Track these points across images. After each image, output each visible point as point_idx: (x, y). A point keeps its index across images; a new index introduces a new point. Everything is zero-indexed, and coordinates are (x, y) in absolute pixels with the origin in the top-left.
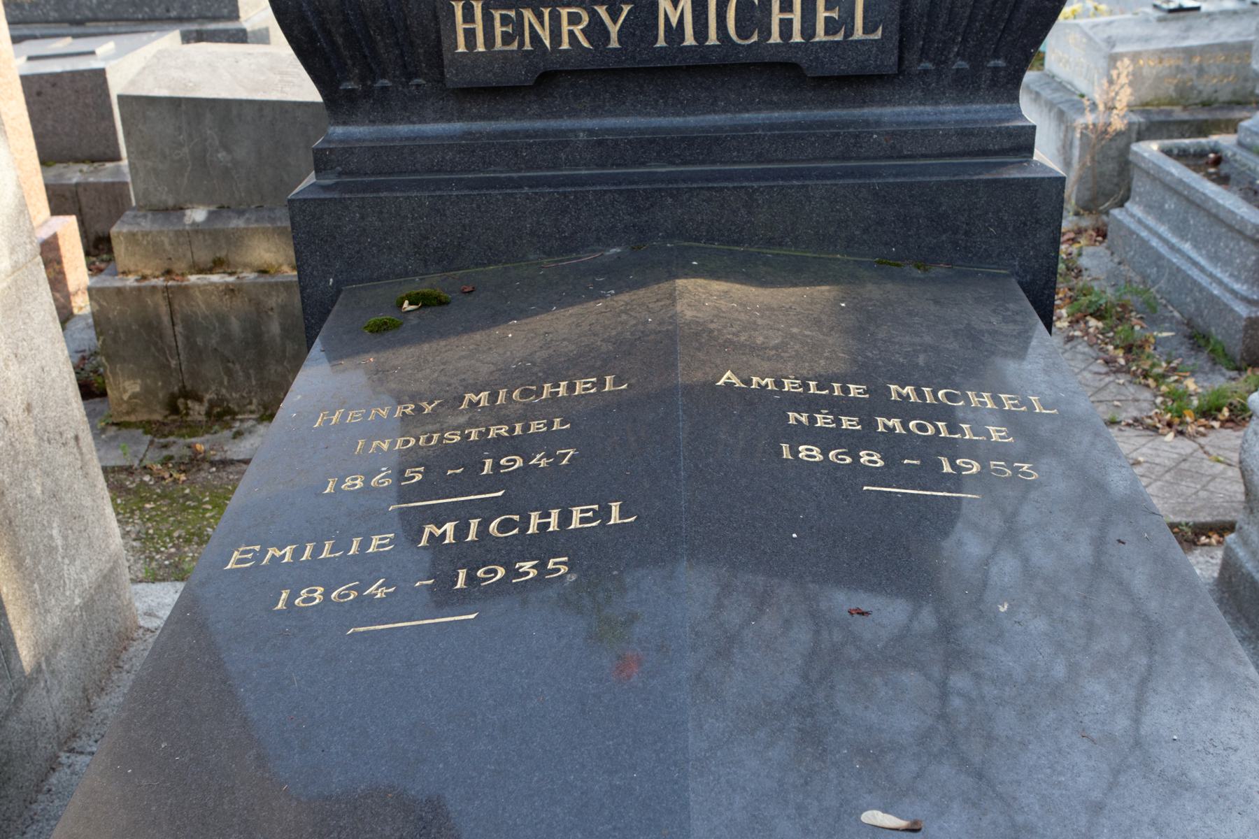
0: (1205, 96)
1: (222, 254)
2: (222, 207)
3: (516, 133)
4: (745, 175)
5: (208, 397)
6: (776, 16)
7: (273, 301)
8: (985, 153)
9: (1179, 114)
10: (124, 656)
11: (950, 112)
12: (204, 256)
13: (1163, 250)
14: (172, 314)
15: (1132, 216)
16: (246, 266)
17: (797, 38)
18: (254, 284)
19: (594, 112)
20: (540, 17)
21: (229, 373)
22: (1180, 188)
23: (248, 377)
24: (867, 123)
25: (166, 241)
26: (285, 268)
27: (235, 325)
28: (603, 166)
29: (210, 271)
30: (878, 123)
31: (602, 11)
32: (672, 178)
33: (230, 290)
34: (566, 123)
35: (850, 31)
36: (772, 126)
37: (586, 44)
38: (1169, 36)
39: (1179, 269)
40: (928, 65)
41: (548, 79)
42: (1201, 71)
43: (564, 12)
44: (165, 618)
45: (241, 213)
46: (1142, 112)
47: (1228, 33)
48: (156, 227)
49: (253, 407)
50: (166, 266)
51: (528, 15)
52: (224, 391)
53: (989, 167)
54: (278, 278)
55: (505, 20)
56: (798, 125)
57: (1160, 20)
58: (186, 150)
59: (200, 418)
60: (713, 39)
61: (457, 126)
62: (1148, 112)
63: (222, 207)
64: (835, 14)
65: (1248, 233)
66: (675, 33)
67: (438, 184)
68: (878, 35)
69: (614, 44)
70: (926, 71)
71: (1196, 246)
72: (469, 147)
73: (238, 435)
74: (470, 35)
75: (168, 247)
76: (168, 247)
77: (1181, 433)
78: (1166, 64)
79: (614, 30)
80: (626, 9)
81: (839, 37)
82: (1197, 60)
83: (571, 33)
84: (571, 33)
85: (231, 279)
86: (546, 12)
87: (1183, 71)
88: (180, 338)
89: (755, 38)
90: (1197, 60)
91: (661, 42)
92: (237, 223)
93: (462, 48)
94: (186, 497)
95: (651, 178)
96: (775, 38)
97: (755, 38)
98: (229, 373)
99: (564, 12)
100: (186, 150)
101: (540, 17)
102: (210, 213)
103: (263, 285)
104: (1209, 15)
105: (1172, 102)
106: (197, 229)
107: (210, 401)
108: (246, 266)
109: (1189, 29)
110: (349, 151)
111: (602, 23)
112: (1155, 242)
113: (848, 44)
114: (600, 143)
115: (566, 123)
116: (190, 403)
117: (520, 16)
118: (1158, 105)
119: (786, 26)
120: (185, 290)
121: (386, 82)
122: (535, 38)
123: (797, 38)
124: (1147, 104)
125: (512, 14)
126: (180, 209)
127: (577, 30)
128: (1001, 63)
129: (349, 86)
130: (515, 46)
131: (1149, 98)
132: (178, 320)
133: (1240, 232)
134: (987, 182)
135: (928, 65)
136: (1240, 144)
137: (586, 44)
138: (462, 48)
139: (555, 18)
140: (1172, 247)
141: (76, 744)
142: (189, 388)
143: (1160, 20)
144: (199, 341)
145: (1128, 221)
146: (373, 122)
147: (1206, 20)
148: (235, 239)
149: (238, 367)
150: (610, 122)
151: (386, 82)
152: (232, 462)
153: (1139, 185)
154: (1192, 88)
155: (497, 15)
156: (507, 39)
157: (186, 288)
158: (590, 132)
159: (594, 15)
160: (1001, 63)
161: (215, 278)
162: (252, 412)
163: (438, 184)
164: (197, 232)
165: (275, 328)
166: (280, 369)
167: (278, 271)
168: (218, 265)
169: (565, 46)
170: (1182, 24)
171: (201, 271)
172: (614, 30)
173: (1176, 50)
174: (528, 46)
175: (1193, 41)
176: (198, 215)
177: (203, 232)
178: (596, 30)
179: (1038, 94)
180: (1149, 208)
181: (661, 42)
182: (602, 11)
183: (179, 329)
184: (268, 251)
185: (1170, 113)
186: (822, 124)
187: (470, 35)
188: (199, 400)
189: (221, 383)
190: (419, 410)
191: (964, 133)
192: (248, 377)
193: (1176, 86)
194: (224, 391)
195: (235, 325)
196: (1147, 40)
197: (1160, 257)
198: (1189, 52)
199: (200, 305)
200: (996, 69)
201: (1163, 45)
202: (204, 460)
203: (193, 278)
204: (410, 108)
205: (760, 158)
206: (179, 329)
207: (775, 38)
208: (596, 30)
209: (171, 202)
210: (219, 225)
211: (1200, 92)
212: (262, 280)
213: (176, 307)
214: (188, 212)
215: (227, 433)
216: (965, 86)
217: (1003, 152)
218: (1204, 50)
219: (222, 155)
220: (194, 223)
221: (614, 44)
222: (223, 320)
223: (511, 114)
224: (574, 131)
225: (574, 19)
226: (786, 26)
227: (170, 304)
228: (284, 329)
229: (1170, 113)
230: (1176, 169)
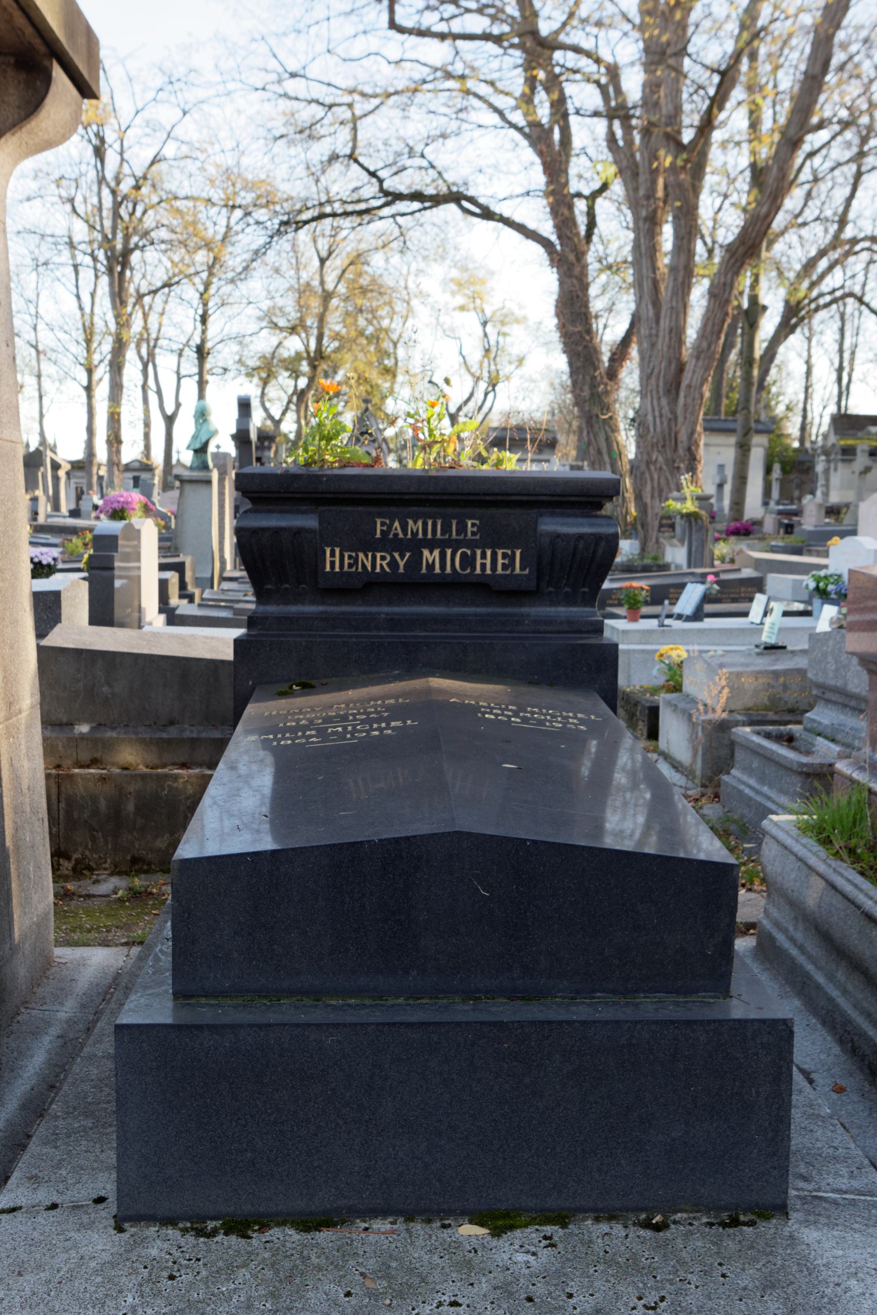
0: (790, 706)
1: (98, 755)
2: (100, 725)
3: (350, 613)
4: (463, 637)
5: (75, 856)
6: (479, 561)
7: (132, 788)
8: (580, 632)
9: (771, 716)
10: (48, 973)
11: (562, 611)
12: (85, 756)
13: (751, 794)
14: (59, 794)
15: (735, 777)
16: (113, 764)
17: (488, 571)
18: (120, 775)
19: (389, 604)
20: (367, 556)
21: (93, 839)
22: (759, 750)
23: (106, 843)
24: (522, 615)
25: (60, 744)
26: (141, 767)
27: (103, 804)
28: (392, 631)
29: (88, 767)
30: (528, 615)
31: (396, 555)
32: (426, 637)
33: (103, 779)
34: (374, 609)
35: (513, 569)
36: (476, 615)
37: (387, 570)
38: (766, 663)
39: (760, 804)
40: (551, 589)
41: (370, 586)
42: (785, 687)
43: (378, 555)
44: (684, 130)
45: (113, 728)
46: (745, 715)
47: (801, 663)
48: (54, 735)
49: (107, 866)
50: (57, 762)
51: (361, 555)
52: (87, 852)
53: (581, 638)
54: (137, 772)
55: (350, 557)
56: (489, 615)
57: (758, 654)
58: (81, 684)
59: (67, 872)
60: (448, 570)
61: (321, 608)
62: (750, 715)
63: (100, 725)
64: (506, 562)
65: (795, 768)
66: (431, 567)
67: (310, 636)
68: (527, 572)
69: (401, 570)
70: (551, 592)
71: (771, 787)
72: (324, 618)
73: (96, 882)
74: (333, 563)
75: (61, 748)
76: (61, 748)
77: (750, 890)
78: (761, 681)
79: (402, 564)
80: (408, 555)
81: (508, 572)
82: (782, 680)
83: (381, 565)
84: (381, 565)
85: (104, 771)
86: (370, 555)
87: (773, 687)
88: (62, 812)
89: (468, 571)
90: (782, 680)
91: (424, 571)
92: (111, 734)
93: (328, 569)
94: (66, 911)
95: (416, 637)
96: (478, 571)
97: (468, 571)
98: (93, 839)
99: (378, 555)
100: (81, 684)
101: (367, 556)
102: (92, 729)
103: (126, 776)
104: (793, 652)
105: (767, 709)
106: (83, 737)
107: (76, 860)
108: (113, 764)
109: (777, 660)
110: (266, 618)
111: (396, 561)
112: (747, 791)
113: (512, 576)
114: (392, 619)
115: (374, 609)
116: (61, 860)
117: (357, 556)
118: (757, 710)
119: (483, 566)
120: (71, 777)
121: (287, 586)
122: (364, 566)
123: (488, 571)
124: (749, 709)
125: (354, 554)
126: (70, 724)
127: (384, 563)
128: (586, 590)
129: (269, 587)
130: (354, 569)
131: (750, 705)
132: (62, 799)
133: (791, 770)
134: (581, 645)
135: (551, 589)
136: (806, 729)
137: (387, 570)
138: (328, 569)
139: (374, 558)
140: (758, 792)
141: (29, 1006)
142: (62, 849)
143: (758, 654)
144: (76, 815)
145: (734, 783)
146: (278, 604)
147: (790, 655)
148: (109, 745)
149: (100, 835)
150: (396, 609)
151: (287, 586)
152: (94, 896)
153: (739, 755)
154: (780, 699)
155: (346, 555)
156: (350, 566)
157: (73, 775)
158: (387, 614)
159: (392, 557)
160: (586, 590)
161: (92, 771)
162: (106, 869)
163: (310, 636)
164: (82, 739)
165: (131, 807)
166: (130, 837)
167: (135, 769)
168: (94, 762)
169: (378, 570)
170: (773, 657)
171: (81, 767)
172: (402, 564)
173: (766, 672)
174: (360, 570)
175: (779, 667)
176: (85, 728)
177: (87, 739)
178: (393, 564)
179: (676, 706)
180: (744, 770)
181: (424, 571)
182: (396, 555)
183: (62, 805)
184: (131, 754)
185: (766, 715)
186: (500, 615)
187: (333, 563)
188: (69, 858)
189: (86, 846)
190: (304, 733)
191: (569, 622)
192: (106, 843)
193: (769, 697)
194: (87, 852)
195: (103, 804)
196: (747, 665)
197: (750, 799)
198: (776, 674)
199: (80, 789)
200: (584, 593)
201: (757, 668)
202: (73, 894)
203: (77, 771)
204: (298, 599)
205: (469, 631)
206: (62, 805)
207: (478, 571)
208: (393, 564)
209: (65, 720)
210: (98, 735)
211: (786, 702)
212: (125, 772)
213: (63, 789)
214: (77, 727)
215: (89, 881)
216: (570, 600)
217: (588, 632)
218: (786, 672)
219: (105, 689)
220: (81, 733)
221: (401, 570)
222: (94, 799)
223: (348, 604)
224: (379, 613)
225: (383, 558)
226: (483, 566)
227: (59, 787)
228: (137, 809)
229: (766, 715)
230: (756, 739)
